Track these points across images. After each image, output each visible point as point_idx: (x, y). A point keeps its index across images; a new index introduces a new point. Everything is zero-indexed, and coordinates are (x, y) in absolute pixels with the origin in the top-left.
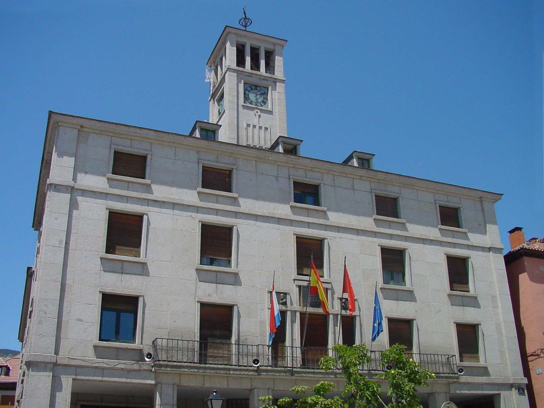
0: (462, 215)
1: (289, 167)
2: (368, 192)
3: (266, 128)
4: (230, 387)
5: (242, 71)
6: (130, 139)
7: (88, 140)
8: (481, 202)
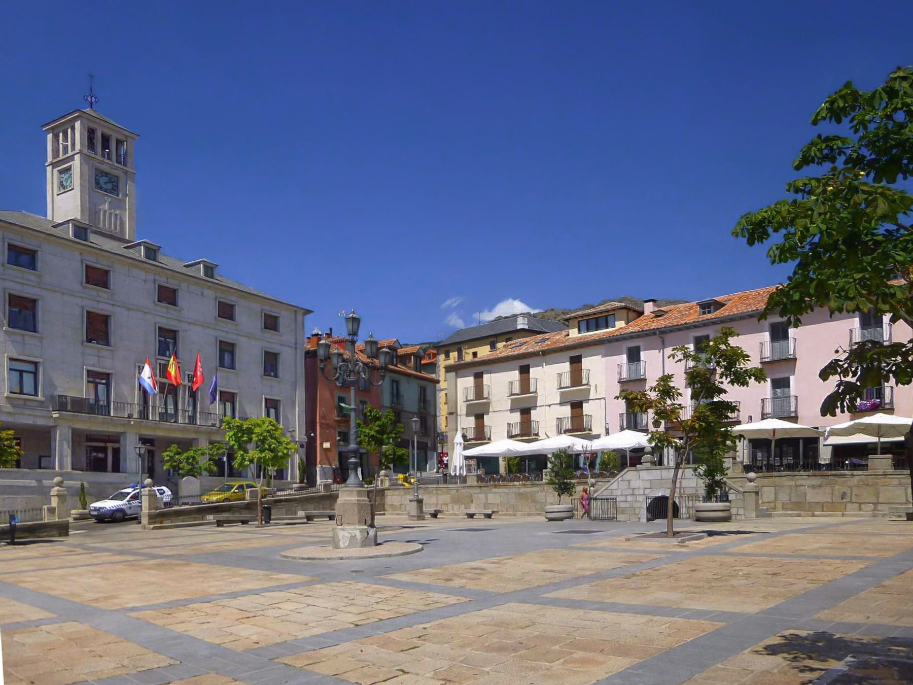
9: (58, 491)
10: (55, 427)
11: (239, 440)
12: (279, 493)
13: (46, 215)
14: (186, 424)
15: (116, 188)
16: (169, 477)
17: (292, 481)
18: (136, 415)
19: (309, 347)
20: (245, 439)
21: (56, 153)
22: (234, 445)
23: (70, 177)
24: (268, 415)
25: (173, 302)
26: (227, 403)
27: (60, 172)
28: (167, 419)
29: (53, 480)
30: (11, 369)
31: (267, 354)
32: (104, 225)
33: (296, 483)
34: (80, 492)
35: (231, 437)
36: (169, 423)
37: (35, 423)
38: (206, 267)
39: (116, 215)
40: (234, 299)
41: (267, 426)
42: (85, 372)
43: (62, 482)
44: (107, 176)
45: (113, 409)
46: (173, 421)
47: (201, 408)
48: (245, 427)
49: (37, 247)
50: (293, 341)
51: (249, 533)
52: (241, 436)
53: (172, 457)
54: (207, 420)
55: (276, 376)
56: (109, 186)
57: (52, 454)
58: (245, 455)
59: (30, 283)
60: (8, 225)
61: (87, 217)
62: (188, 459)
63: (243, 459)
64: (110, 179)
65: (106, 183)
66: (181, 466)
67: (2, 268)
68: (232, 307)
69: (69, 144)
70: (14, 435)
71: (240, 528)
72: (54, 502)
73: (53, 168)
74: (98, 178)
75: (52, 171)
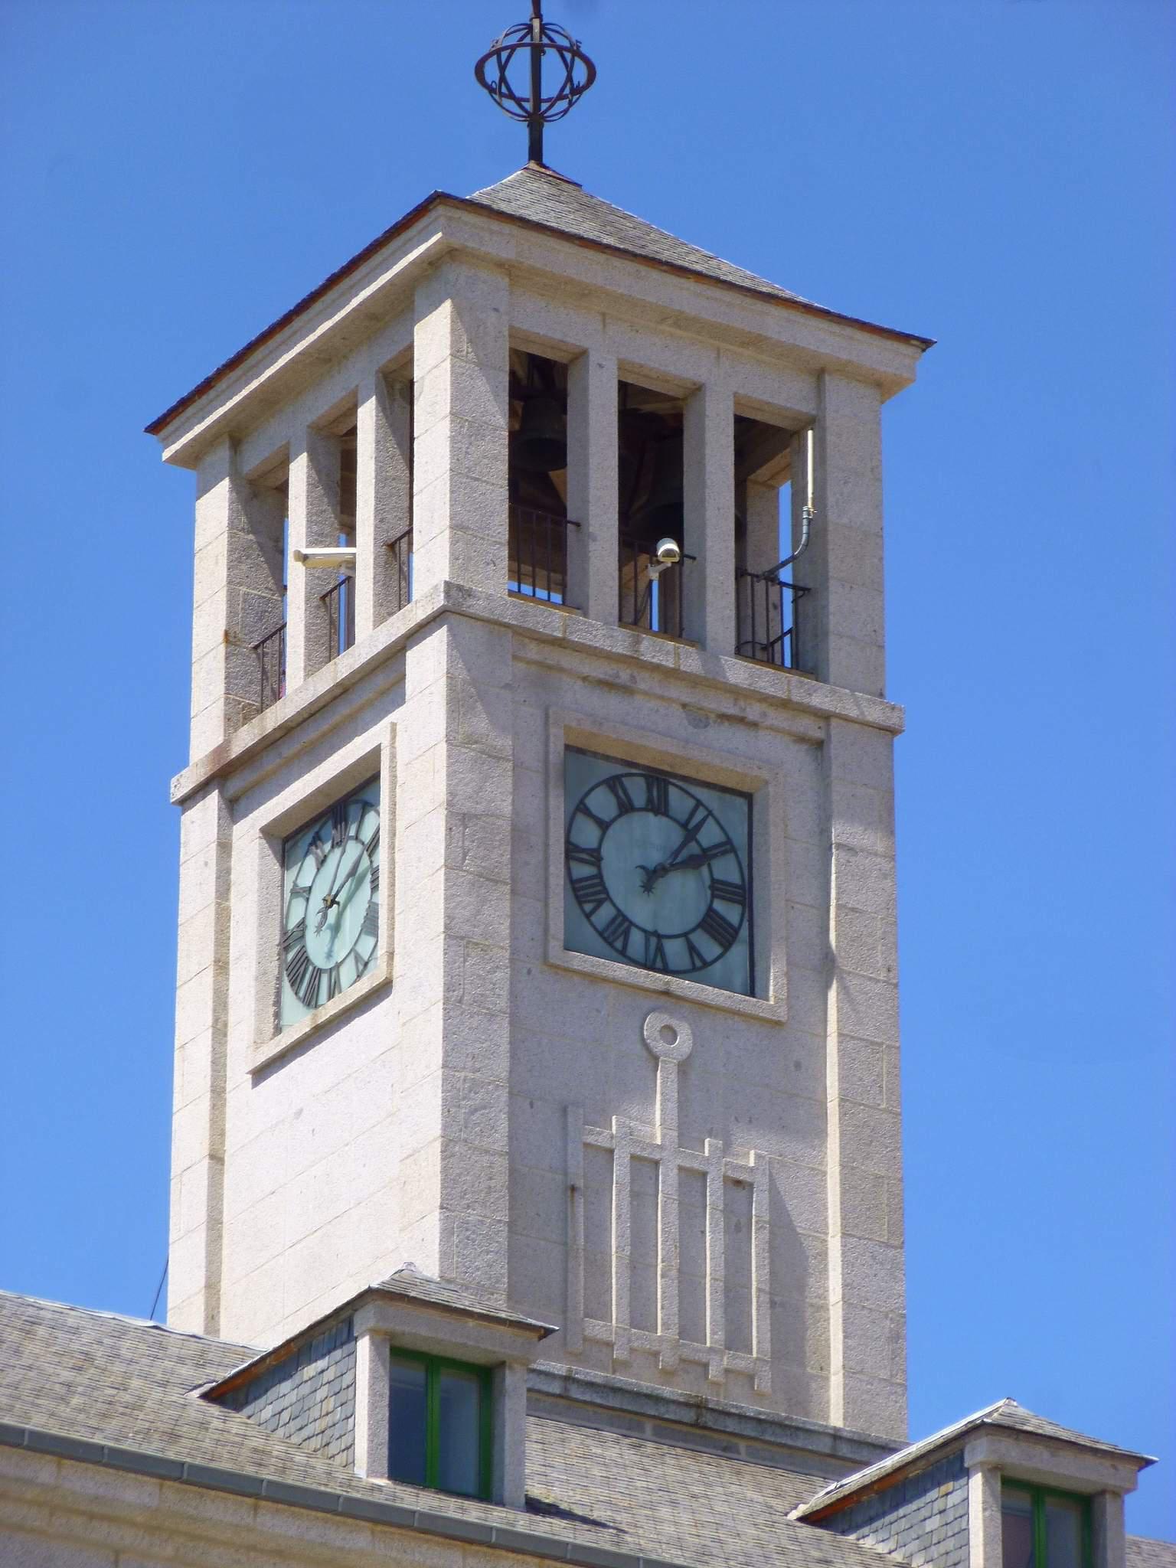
3: (738, 1183)
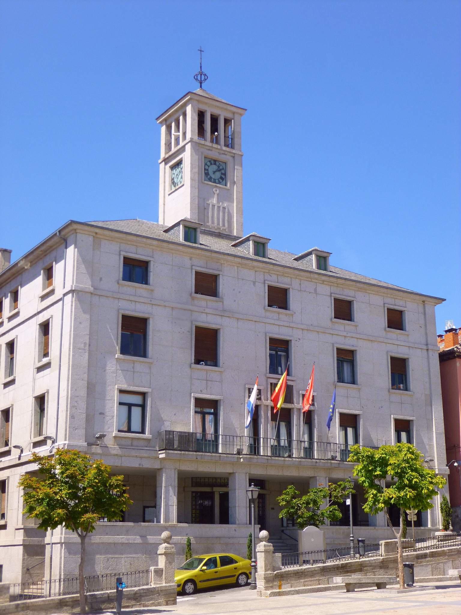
0: (407, 317)
1: (264, 272)
2: (328, 296)
3: (224, 208)
4: (217, 471)
5: (204, 145)
6: (135, 245)
7: (100, 246)
8: (424, 305)
9: (166, 548)
10: (160, 470)
11: (371, 474)
12: (419, 545)
13: (157, 221)
14: (302, 458)
15: (223, 176)
16: (283, 528)
17: (434, 528)
18: (246, 450)
19: (443, 347)
20: (378, 473)
21: (168, 146)
22: (364, 482)
23: (181, 172)
24: (399, 440)
25: (144, 279)
26: (402, 433)
27: (173, 168)
28: (279, 454)
29: (160, 535)
30: (120, 404)
31: (393, 359)
32: (213, 222)
33: (438, 530)
34: (186, 550)
35: (360, 471)
36: (283, 459)
37: (141, 466)
38: (319, 258)
39: (224, 208)
40: (352, 293)
41: (405, 455)
42: (193, 401)
43: (170, 537)
44: (215, 164)
45: (222, 444)
46: (286, 455)
47: (319, 437)
48: (377, 457)
49: (289, 285)
50: (423, 341)
51: (392, 601)
52: (367, 474)
53: (288, 502)
54: (325, 451)
55: (406, 389)
56: (218, 175)
57: (158, 504)
58: (378, 495)
59: (142, 300)
60: (124, 236)
61: (196, 216)
62: (308, 503)
63: (376, 500)
64: (219, 167)
65: (214, 172)
66: (300, 513)
67: (117, 286)
68: (284, 292)
69: (181, 134)
70: (123, 481)
71: (376, 593)
72: (162, 562)
73: (166, 164)
74: (207, 167)
75: (165, 168)
